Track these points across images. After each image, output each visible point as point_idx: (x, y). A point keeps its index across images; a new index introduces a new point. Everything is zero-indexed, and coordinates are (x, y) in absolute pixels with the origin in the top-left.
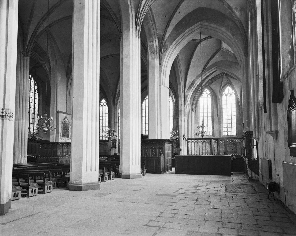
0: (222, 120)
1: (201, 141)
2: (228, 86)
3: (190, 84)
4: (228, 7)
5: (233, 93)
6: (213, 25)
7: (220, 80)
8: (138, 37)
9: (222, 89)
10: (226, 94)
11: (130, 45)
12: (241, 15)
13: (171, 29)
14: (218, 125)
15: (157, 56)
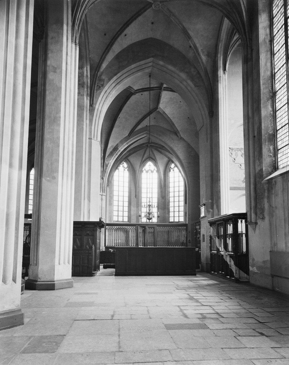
0: (141, 203)
1: (116, 227)
2: (149, 161)
3: (112, 149)
4: (193, 45)
5: (154, 170)
6: (170, 67)
7: (142, 152)
8: (76, 44)
9: (143, 163)
10: (147, 170)
11: (61, 51)
12: (208, 61)
13: (110, 57)
14: (136, 208)
15: (87, 91)
